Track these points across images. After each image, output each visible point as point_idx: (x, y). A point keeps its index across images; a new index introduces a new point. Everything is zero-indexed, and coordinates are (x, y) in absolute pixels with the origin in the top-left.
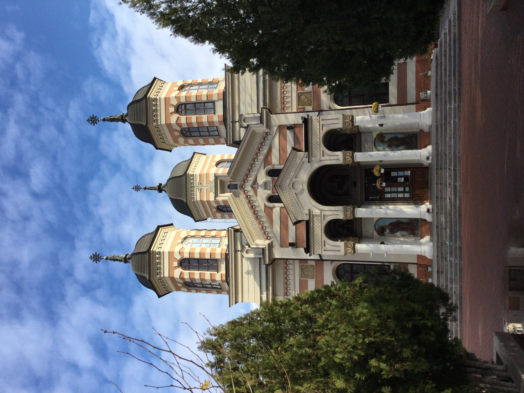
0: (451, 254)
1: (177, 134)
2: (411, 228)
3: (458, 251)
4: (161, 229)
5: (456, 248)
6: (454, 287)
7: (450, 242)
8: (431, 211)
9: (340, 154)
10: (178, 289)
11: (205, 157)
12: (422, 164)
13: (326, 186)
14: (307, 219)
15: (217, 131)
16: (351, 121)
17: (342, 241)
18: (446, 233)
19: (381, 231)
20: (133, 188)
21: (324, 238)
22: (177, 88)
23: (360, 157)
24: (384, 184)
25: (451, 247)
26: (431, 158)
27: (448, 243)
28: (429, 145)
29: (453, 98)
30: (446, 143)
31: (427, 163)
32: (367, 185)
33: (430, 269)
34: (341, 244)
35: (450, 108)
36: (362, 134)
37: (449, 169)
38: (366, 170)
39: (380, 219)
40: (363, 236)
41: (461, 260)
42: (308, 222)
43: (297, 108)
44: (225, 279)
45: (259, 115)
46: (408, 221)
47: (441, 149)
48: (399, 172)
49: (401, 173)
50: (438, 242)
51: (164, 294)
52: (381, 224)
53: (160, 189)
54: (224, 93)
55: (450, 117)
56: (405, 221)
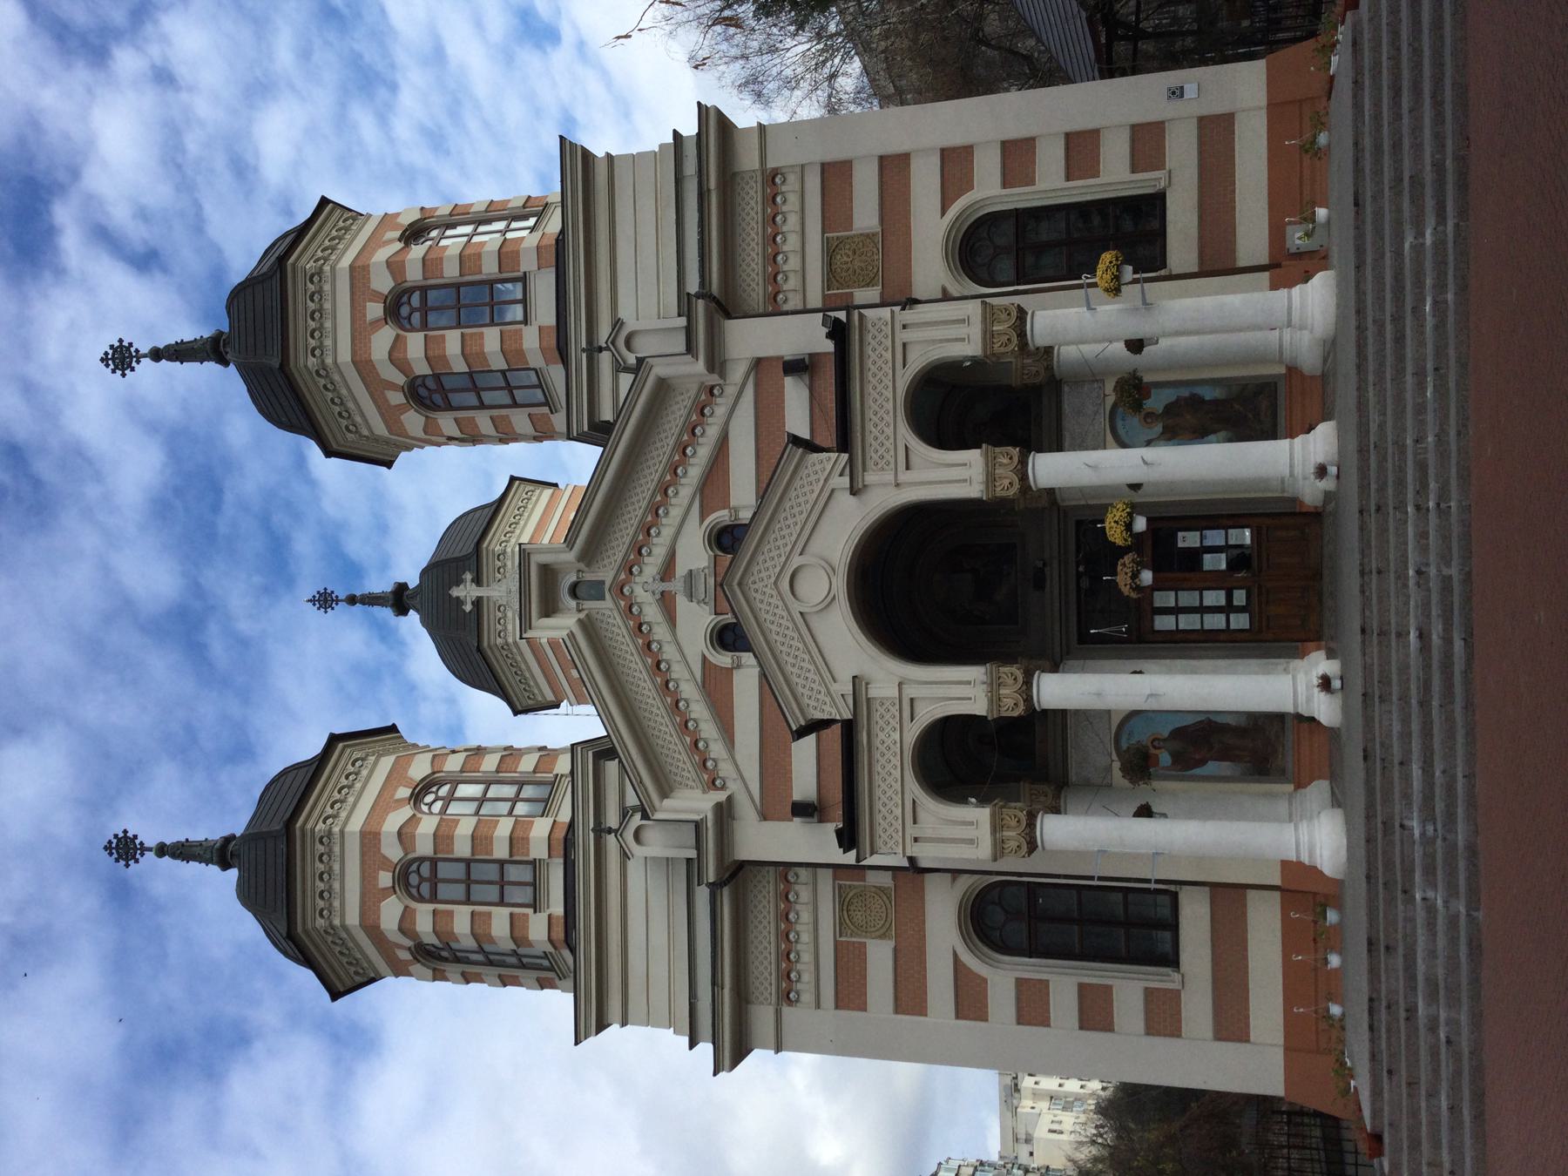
0: (1429, 870)
1: (397, 398)
2: (1251, 751)
3: (1462, 864)
4: (341, 745)
5: (1451, 849)
6: (1443, 1015)
7: (1423, 822)
8: (1336, 684)
9: (973, 458)
10: (400, 970)
11: (548, 492)
12: (1295, 500)
13: (920, 584)
14: (848, 715)
15: (540, 386)
16: (1013, 327)
17: (983, 801)
18: (1407, 778)
19: (1139, 766)
20: (312, 601)
21: (914, 788)
22: (398, 234)
23: (1053, 469)
24: (1147, 577)
25: (1427, 841)
26: (1333, 470)
27: (1415, 825)
28: (1324, 420)
29: (1430, 203)
30: (1399, 398)
31: (1311, 491)
32: (1085, 583)
33: (1332, 916)
34: (977, 817)
35: (1418, 249)
36: (1066, 389)
37: (1418, 508)
38: (1079, 523)
39: (1134, 714)
40: (1073, 777)
41: (1473, 903)
42: (849, 728)
43: (824, 297)
44: (562, 936)
45: (683, 321)
46: (1243, 722)
47: (1382, 426)
48: (1208, 533)
49: (1215, 537)
50: (1369, 817)
51: (349, 984)
52: (1141, 734)
53: (400, 600)
54: (561, 241)
55: (1419, 283)
56: (1231, 721)
